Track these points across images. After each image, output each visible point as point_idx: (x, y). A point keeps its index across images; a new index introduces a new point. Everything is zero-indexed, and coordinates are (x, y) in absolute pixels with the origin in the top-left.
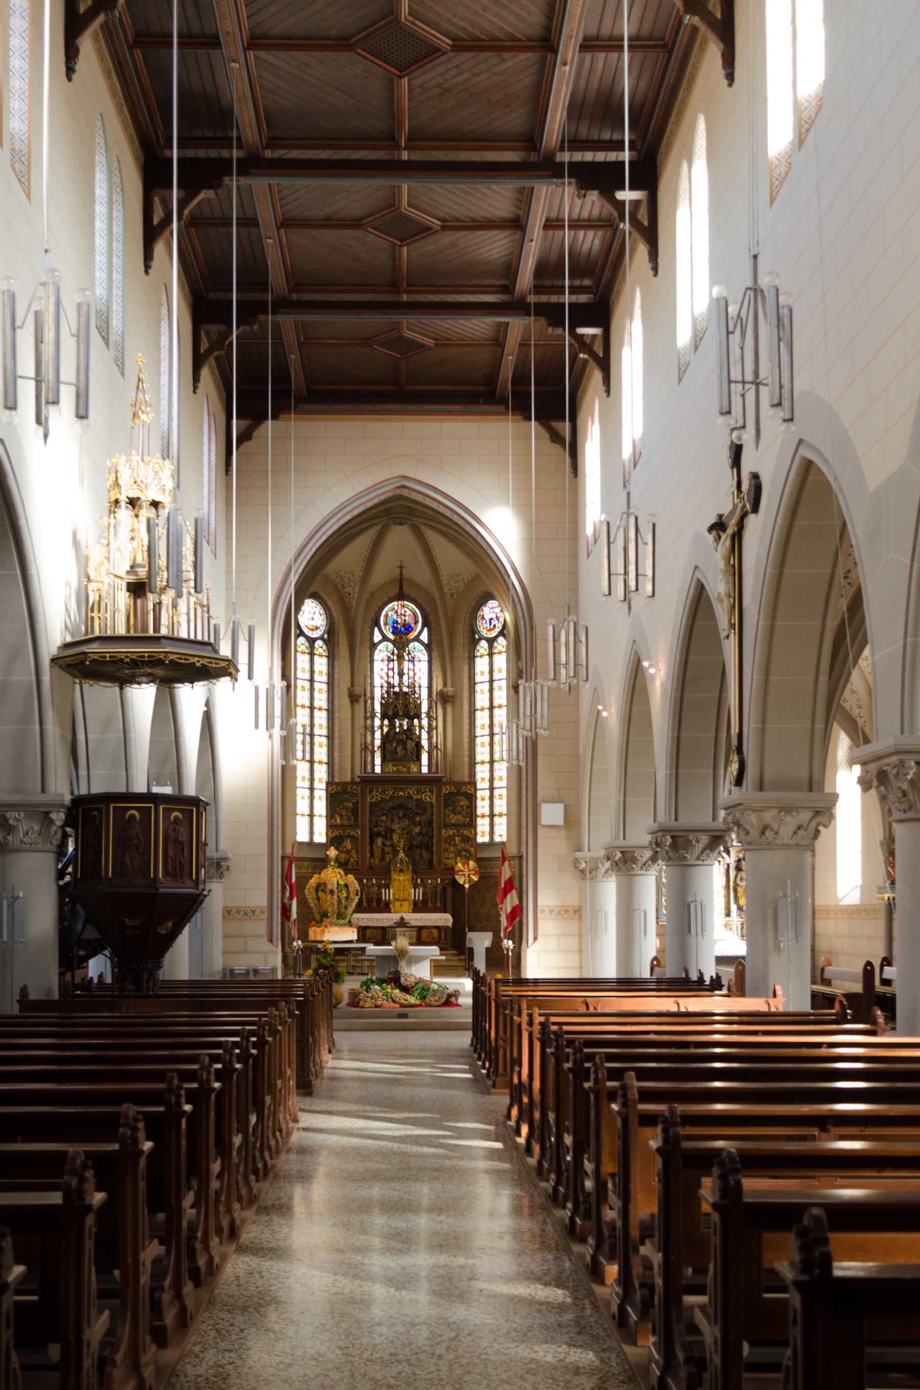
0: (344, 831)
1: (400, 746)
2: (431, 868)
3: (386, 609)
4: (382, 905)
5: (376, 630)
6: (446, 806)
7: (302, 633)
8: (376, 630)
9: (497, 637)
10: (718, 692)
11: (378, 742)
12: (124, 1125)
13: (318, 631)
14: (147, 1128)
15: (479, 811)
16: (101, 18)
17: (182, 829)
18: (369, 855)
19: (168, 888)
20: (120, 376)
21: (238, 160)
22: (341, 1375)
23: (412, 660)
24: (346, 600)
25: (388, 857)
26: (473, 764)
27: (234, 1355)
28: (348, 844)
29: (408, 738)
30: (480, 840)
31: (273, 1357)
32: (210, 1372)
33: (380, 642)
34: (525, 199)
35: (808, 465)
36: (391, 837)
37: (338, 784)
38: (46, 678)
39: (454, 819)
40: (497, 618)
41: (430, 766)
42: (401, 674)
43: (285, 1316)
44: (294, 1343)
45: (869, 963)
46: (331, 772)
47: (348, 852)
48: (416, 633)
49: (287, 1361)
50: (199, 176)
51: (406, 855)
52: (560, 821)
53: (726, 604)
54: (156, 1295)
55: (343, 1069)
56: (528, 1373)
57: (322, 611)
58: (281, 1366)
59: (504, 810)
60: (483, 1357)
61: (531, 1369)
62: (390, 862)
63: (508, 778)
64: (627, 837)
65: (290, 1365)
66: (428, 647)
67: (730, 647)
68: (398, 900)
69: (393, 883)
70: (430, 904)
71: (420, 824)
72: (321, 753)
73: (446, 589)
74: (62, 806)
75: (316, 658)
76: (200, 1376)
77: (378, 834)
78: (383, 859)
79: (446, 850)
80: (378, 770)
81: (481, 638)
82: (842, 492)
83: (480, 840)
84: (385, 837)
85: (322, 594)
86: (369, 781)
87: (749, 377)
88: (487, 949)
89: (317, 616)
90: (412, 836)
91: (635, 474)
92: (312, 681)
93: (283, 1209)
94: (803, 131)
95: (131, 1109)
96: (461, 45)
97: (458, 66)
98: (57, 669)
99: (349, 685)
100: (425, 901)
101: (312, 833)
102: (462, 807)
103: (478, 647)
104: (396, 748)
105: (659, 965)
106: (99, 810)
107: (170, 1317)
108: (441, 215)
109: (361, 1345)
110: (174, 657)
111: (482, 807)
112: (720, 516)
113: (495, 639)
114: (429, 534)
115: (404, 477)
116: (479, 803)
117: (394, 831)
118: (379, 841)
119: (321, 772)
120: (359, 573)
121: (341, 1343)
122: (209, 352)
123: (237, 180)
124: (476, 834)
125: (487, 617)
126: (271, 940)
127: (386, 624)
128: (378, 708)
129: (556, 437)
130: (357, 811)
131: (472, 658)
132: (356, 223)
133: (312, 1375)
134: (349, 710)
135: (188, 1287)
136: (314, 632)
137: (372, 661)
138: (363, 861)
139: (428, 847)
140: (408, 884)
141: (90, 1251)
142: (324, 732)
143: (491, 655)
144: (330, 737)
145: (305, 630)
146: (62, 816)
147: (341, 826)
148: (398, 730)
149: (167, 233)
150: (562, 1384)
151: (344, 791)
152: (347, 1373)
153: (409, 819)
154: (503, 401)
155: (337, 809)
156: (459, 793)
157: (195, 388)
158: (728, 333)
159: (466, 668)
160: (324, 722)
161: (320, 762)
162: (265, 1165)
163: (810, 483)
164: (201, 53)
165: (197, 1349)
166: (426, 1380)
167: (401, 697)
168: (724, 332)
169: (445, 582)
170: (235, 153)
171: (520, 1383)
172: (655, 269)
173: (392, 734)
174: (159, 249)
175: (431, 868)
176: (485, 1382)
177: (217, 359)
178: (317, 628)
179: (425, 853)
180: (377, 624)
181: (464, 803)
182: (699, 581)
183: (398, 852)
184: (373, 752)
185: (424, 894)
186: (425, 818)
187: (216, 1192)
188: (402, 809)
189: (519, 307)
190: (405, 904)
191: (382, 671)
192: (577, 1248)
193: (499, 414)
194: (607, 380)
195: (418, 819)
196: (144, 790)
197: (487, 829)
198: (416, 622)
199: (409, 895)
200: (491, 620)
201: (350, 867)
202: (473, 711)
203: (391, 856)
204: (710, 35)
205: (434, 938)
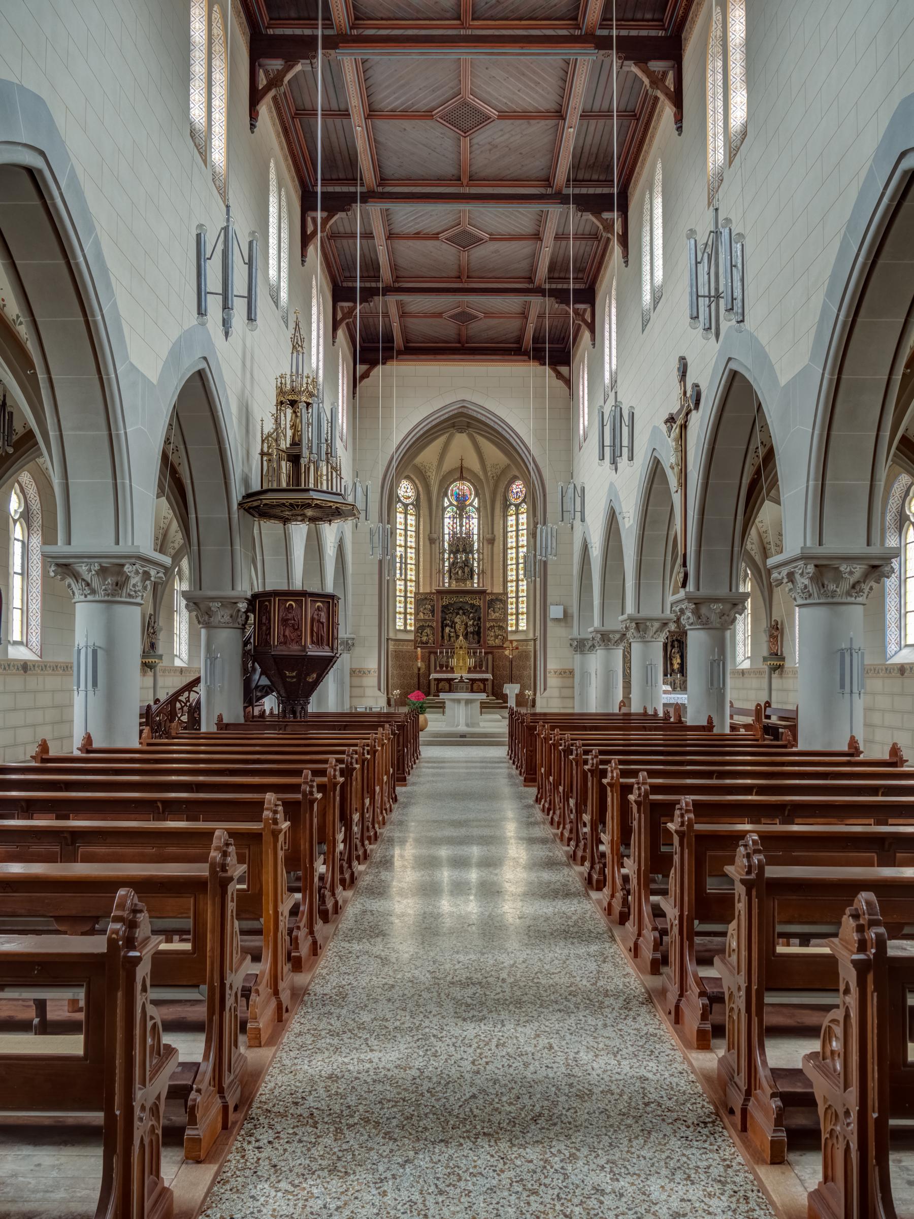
1: (462, 570)
6: (489, 608)
7: (400, 501)
8: (446, 500)
9: (521, 503)
12: (267, 809)
14: (286, 813)
16: (272, 93)
17: (323, 614)
19: (314, 651)
21: (361, 193)
22: (430, 995)
23: (468, 518)
25: (452, 639)
27: (351, 977)
28: (428, 630)
30: (509, 629)
31: (380, 979)
32: (334, 991)
33: (448, 507)
34: (541, 219)
35: (734, 374)
37: (422, 594)
38: (235, 516)
41: (478, 583)
42: (461, 526)
43: (389, 946)
44: (396, 968)
45: (759, 705)
49: (391, 983)
50: (337, 203)
52: (561, 616)
53: (676, 469)
54: (294, 933)
56: (570, 994)
58: (386, 987)
59: (525, 543)
60: (535, 981)
61: (572, 991)
65: (393, 986)
66: (478, 510)
67: (677, 499)
72: (411, 575)
74: (246, 599)
76: (326, 995)
77: (447, 625)
81: (511, 504)
82: (760, 389)
87: (713, 294)
88: (517, 695)
91: (653, 316)
93: (387, 863)
95: (270, 797)
96: (504, 115)
97: (501, 130)
98: (242, 511)
100: (475, 667)
105: (624, 705)
106: (270, 601)
107: (304, 949)
108: (490, 231)
109: (445, 970)
110: (318, 502)
111: (511, 608)
112: (671, 414)
113: (520, 504)
114: (481, 440)
118: (447, 629)
119: (411, 587)
120: (435, 463)
121: (430, 968)
122: (342, 320)
124: (507, 625)
126: (380, 689)
127: (452, 495)
129: (559, 375)
131: (505, 517)
132: (435, 237)
133: (409, 995)
135: (319, 925)
137: (443, 518)
141: (232, 911)
143: (517, 514)
146: (245, 605)
147: (424, 620)
149: (314, 240)
150: (597, 1004)
152: (435, 994)
154: (526, 353)
158: (697, 263)
160: (413, 523)
162: (376, 833)
163: (736, 388)
164: (338, 121)
165: (324, 972)
166: (494, 999)
168: (693, 262)
169: (489, 469)
170: (359, 189)
171: (565, 1003)
174: (311, 249)
176: (539, 1002)
177: (347, 324)
178: (409, 497)
182: (655, 457)
187: (341, 853)
188: (460, 609)
189: (540, 291)
191: (448, 523)
192: (595, 895)
193: (524, 361)
196: (259, 488)
202: (505, 549)
204: (667, 102)
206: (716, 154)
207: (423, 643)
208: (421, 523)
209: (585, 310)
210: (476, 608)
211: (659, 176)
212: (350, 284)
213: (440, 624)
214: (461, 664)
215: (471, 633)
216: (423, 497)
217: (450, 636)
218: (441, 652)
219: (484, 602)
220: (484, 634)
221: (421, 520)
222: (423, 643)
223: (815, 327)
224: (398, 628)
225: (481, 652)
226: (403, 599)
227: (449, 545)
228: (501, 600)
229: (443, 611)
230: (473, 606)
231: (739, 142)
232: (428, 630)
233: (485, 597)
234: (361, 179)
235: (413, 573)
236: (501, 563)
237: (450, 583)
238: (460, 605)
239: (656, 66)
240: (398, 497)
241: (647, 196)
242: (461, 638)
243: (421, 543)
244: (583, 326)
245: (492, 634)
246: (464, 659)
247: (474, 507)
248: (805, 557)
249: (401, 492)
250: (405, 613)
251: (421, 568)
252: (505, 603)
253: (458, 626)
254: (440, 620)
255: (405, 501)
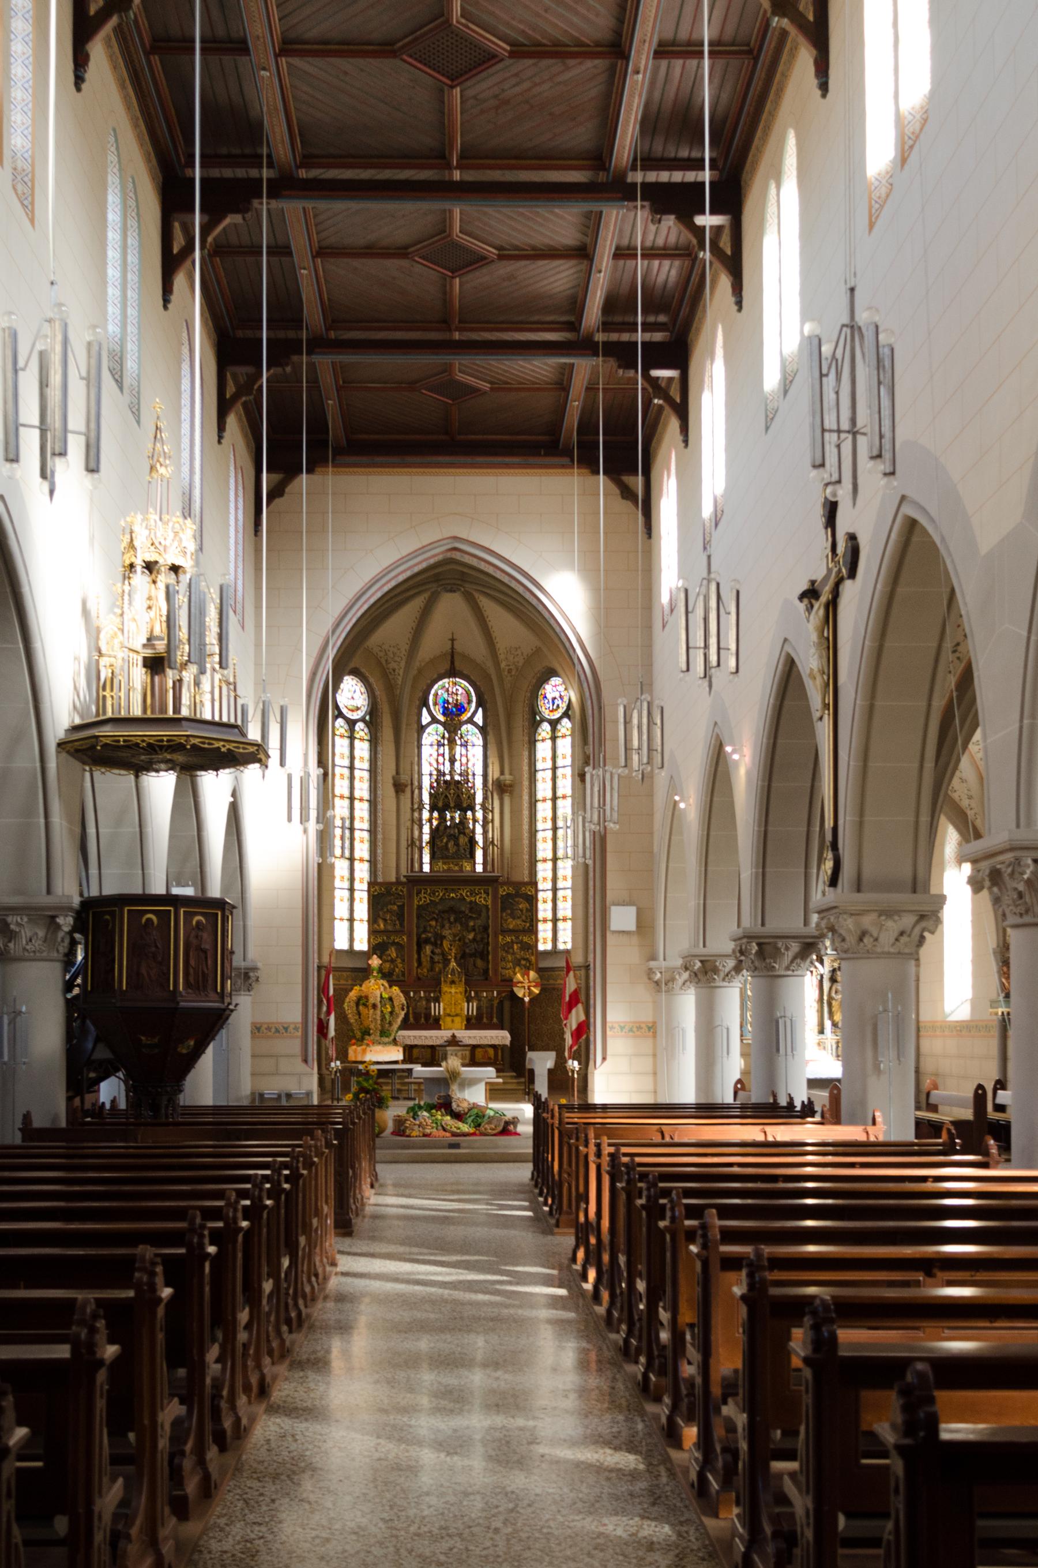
0: (388, 938)
1: (452, 842)
2: (486, 979)
3: (436, 687)
4: (431, 1021)
5: (424, 710)
6: (503, 910)
7: (340, 715)
8: (424, 711)
9: (561, 718)
10: (810, 781)
11: (426, 838)
12: (140, 1270)
13: (359, 712)
14: (166, 1273)
15: (541, 915)
16: (114, 21)
17: (205, 935)
18: (416, 965)
19: (190, 1001)
20: (136, 424)
21: (269, 180)
22: (385, 1551)
23: (465, 745)
24: (391, 677)
25: (438, 967)
26: (533, 861)
27: (263, 1529)
28: (393, 952)
29: (460, 833)
30: (541, 947)
31: (308, 1531)
32: (237, 1547)
33: (429, 724)
34: (593, 224)
35: (912, 525)
36: (442, 944)
37: (381, 884)
38: (52, 764)
39: (512, 924)
40: (561, 697)
41: (485, 864)
42: (452, 761)
43: (321, 1484)
44: (332, 1515)
45: (980, 1087)
46: (373, 871)
47: (392, 961)
48: (469, 715)
49: (324, 1535)
50: (224, 198)
51: (459, 965)
52: (632, 926)
53: (819, 681)
54: (176, 1461)
55: (387, 1206)
56: (595, 1549)
57: (363, 690)
58: (318, 1541)
59: (569, 914)
60: (545, 1530)
61: (599, 1544)
62: (440, 972)
63: (573, 877)
64: (707, 944)
65: (328, 1540)
66: (483, 730)
67: (824, 730)
68: (449, 1015)
69: (443, 996)
70: (485, 1020)
71: (474, 930)
72: (362, 850)
73: (503, 665)
74: (70, 909)
75: (357, 742)
76: (226, 1552)
77: (427, 941)
78: (432, 969)
79: (503, 959)
80: (426, 868)
81: (543, 720)
82: (950, 555)
83: (541, 947)
84: (435, 944)
85: (363, 670)
86: (417, 881)
87: (845, 425)
88: (550, 1071)
89: (358, 695)
90: (465, 943)
91: (716, 535)
92: (352, 768)
93: (320, 1364)
94: (906, 147)
95: (147, 1251)
96: (520, 51)
97: (516, 75)
98: (64, 755)
99: (394, 773)
100: (479, 1016)
101: (351, 940)
102: (521, 911)
103: (540, 730)
104: (447, 844)
105: (743, 1088)
106: (112, 914)
107: (191, 1486)
108: (498, 242)
109: (408, 1517)
110: (196, 741)
111: (544, 910)
112: (813, 582)
113: (558, 721)
114: (484, 602)
115: (455, 538)
116: (541, 906)
117: (445, 937)
118: (428, 949)
119: (362, 871)
120: (405, 647)
121: (385, 1515)
122: (235, 397)
123: (268, 203)
124: (537, 941)
125: (549, 696)
126: (306, 1061)
127: (435, 704)
128: (426, 798)
129: (628, 493)
130: (403, 915)
131: (532, 743)
132: (401, 252)
133: (352, 1552)
134: (394, 801)
135: (212, 1452)
136: (355, 713)
137: (419, 746)
138: (410, 971)
139: (483, 955)
140: (460, 997)
141: (101, 1411)
142: (366, 825)
143: (554, 739)
144: (373, 831)
145: (345, 711)
146: (70, 920)
147: (385, 932)
148: (448, 823)
149: (188, 263)
150: (634, 1561)
151: (389, 892)
152: (391, 1549)
153: (461, 924)
154: (568, 453)
155: (381, 913)
156: (518, 894)
157: (220, 438)
158: (822, 375)
159: (526, 753)
160: (366, 815)
161: (361, 860)
162: (299, 1314)
163: (914, 545)
164: (227, 59)
165: (222, 1521)
166: (481, 1556)
167: (452, 786)
168: (817, 375)
169: (502, 657)
170: (265, 173)
171: (587, 1560)
172: (739, 304)
173: (442, 828)
174: (179, 280)
175: (486, 979)
176: (547, 1559)
177: (245, 405)
178: (358, 709)
179: (479, 963)
180: (425, 704)
181: (523, 905)
182: (788, 655)
183: (449, 961)
184: (421, 849)
185: (478, 1008)
186: (479, 922)
187: (244, 1345)
188: (454, 913)
189: (586, 346)
190: (457, 1020)
191: (431, 756)
192: (651, 1408)
193: (563, 466)
194: (685, 429)
195: (471, 924)
196: (162, 891)
197: (549, 935)
198: (470, 702)
199: (462, 1009)
200: (554, 699)
201: (394, 978)
202: (533, 802)
203: (441, 965)
204: (802, 40)
205: (490, 1058)
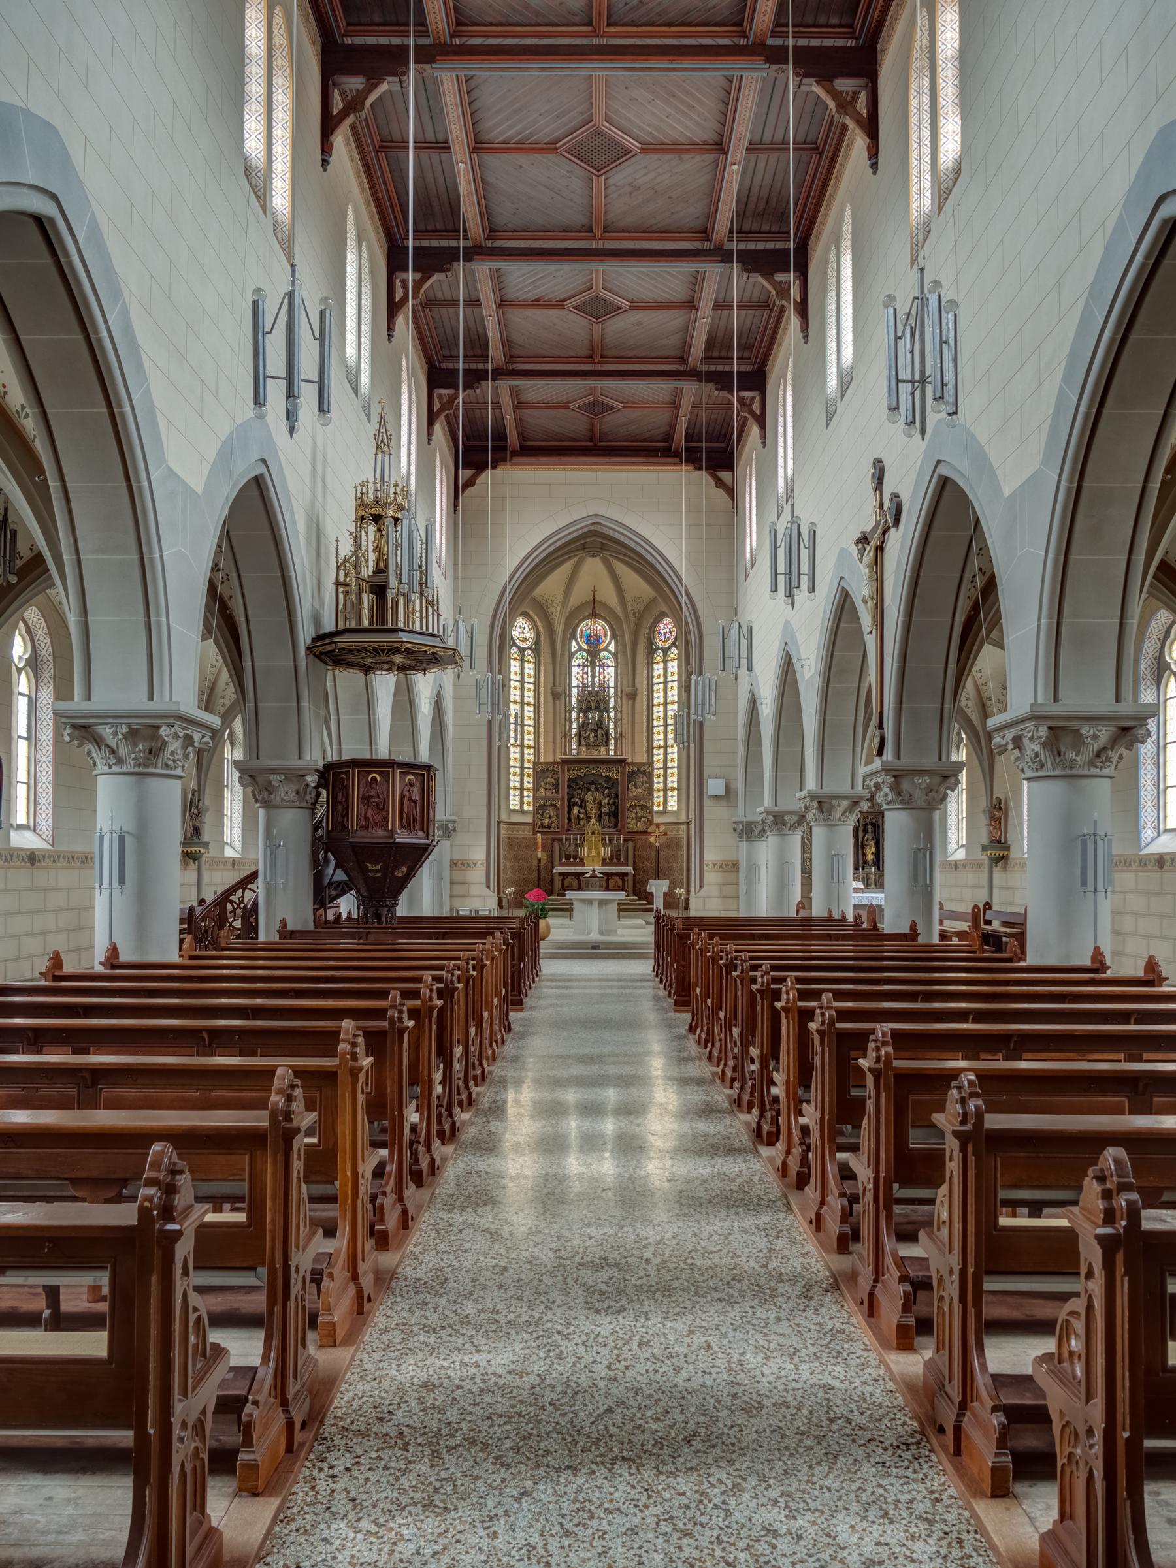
1: (595, 733)
6: (629, 782)
7: (514, 644)
8: (574, 643)
9: (670, 647)
12: (344, 1041)
14: (368, 1045)
16: (350, 119)
17: (415, 790)
19: (403, 838)
21: (464, 248)
22: (554, 1280)
23: (602, 666)
25: (582, 822)
27: (452, 1257)
28: (550, 811)
30: (656, 809)
31: (489, 1259)
32: (429, 1275)
33: (576, 652)
34: (696, 282)
35: (945, 482)
37: (543, 764)
38: (302, 664)
41: (615, 750)
42: (593, 676)
43: (500, 1216)
44: (509, 1245)
45: (976, 907)
49: (503, 1264)
50: (434, 261)
52: (722, 792)
53: (870, 604)
54: (379, 1201)
56: (733, 1279)
58: (497, 1269)
59: (675, 698)
60: (689, 1261)
61: (736, 1275)
65: (505, 1269)
66: (615, 656)
67: (871, 641)
72: (529, 740)
74: (317, 770)
76: (419, 1279)
77: (575, 804)
81: (657, 649)
82: (978, 500)
87: (917, 378)
88: (665, 894)
91: (841, 407)
93: (497, 1110)
95: (347, 1025)
96: (649, 149)
97: (645, 167)
98: (311, 657)
100: (611, 858)
105: (803, 907)
106: (347, 773)
107: (391, 1221)
108: (630, 297)
109: (573, 1247)
110: (409, 646)
111: (658, 783)
112: (864, 533)
113: (669, 649)
114: (619, 566)
118: (576, 810)
119: (529, 755)
120: (560, 596)
121: (553, 1246)
122: (440, 411)
124: (653, 804)
126: (488, 887)
127: (581, 637)
129: (720, 483)
131: (650, 665)
132: (560, 304)
133: (527, 1280)
135: (410, 1190)
137: (570, 667)
141: (299, 1172)
143: (665, 661)
146: (316, 778)
147: (546, 798)
149: (404, 309)
150: (768, 1291)
152: (560, 1278)
154: (677, 454)
158: (897, 338)
160: (532, 672)
162: (483, 1072)
163: (947, 499)
164: (435, 156)
165: (417, 1250)
166: (636, 1286)
168: (892, 337)
169: (629, 604)
170: (462, 243)
171: (727, 1290)
174: (400, 320)
176: (693, 1289)
177: (447, 417)
178: (527, 640)
182: (843, 588)
187: (439, 1097)
188: (592, 783)
189: (694, 374)
191: (577, 673)
192: (765, 1151)
193: (675, 464)
196: (333, 628)
202: (650, 706)
204: (858, 131)
206: (922, 198)
207: (544, 827)
208: (542, 673)
209: (753, 399)
210: (612, 783)
211: (848, 227)
212: (450, 366)
213: (566, 803)
214: (593, 854)
215: (606, 814)
216: (544, 639)
217: (579, 819)
218: (568, 839)
219: (623, 774)
220: (623, 815)
221: (542, 668)
222: (544, 827)
223: (1049, 420)
224: (512, 807)
225: (618, 839)
226: (518, 770)
227: (578, 701)
228: (644, 772)
229: (569, 786)
230: (608, 779)
231: (951, 183)
232: (550, 811)
233: (624, 768)
234: (465, 231)
235: (532, 737)
236: (645, 724)
237: (579, 750)
238: (592, 778)
239: (845, 84)
240: (512, 639)
241: (833, 252)
242: (593, 820)
243: (542, 699)
244: (751, 420)
245: (634, 815)
246: (597, 848)
247: (609, 652)
248: (1036, 717)
249: (516, 633)
250: (522, 789)
251: (542, 730)
252: (649, 775)
253: (589, 806)
254: (566, 797)
255: (520, 644)
